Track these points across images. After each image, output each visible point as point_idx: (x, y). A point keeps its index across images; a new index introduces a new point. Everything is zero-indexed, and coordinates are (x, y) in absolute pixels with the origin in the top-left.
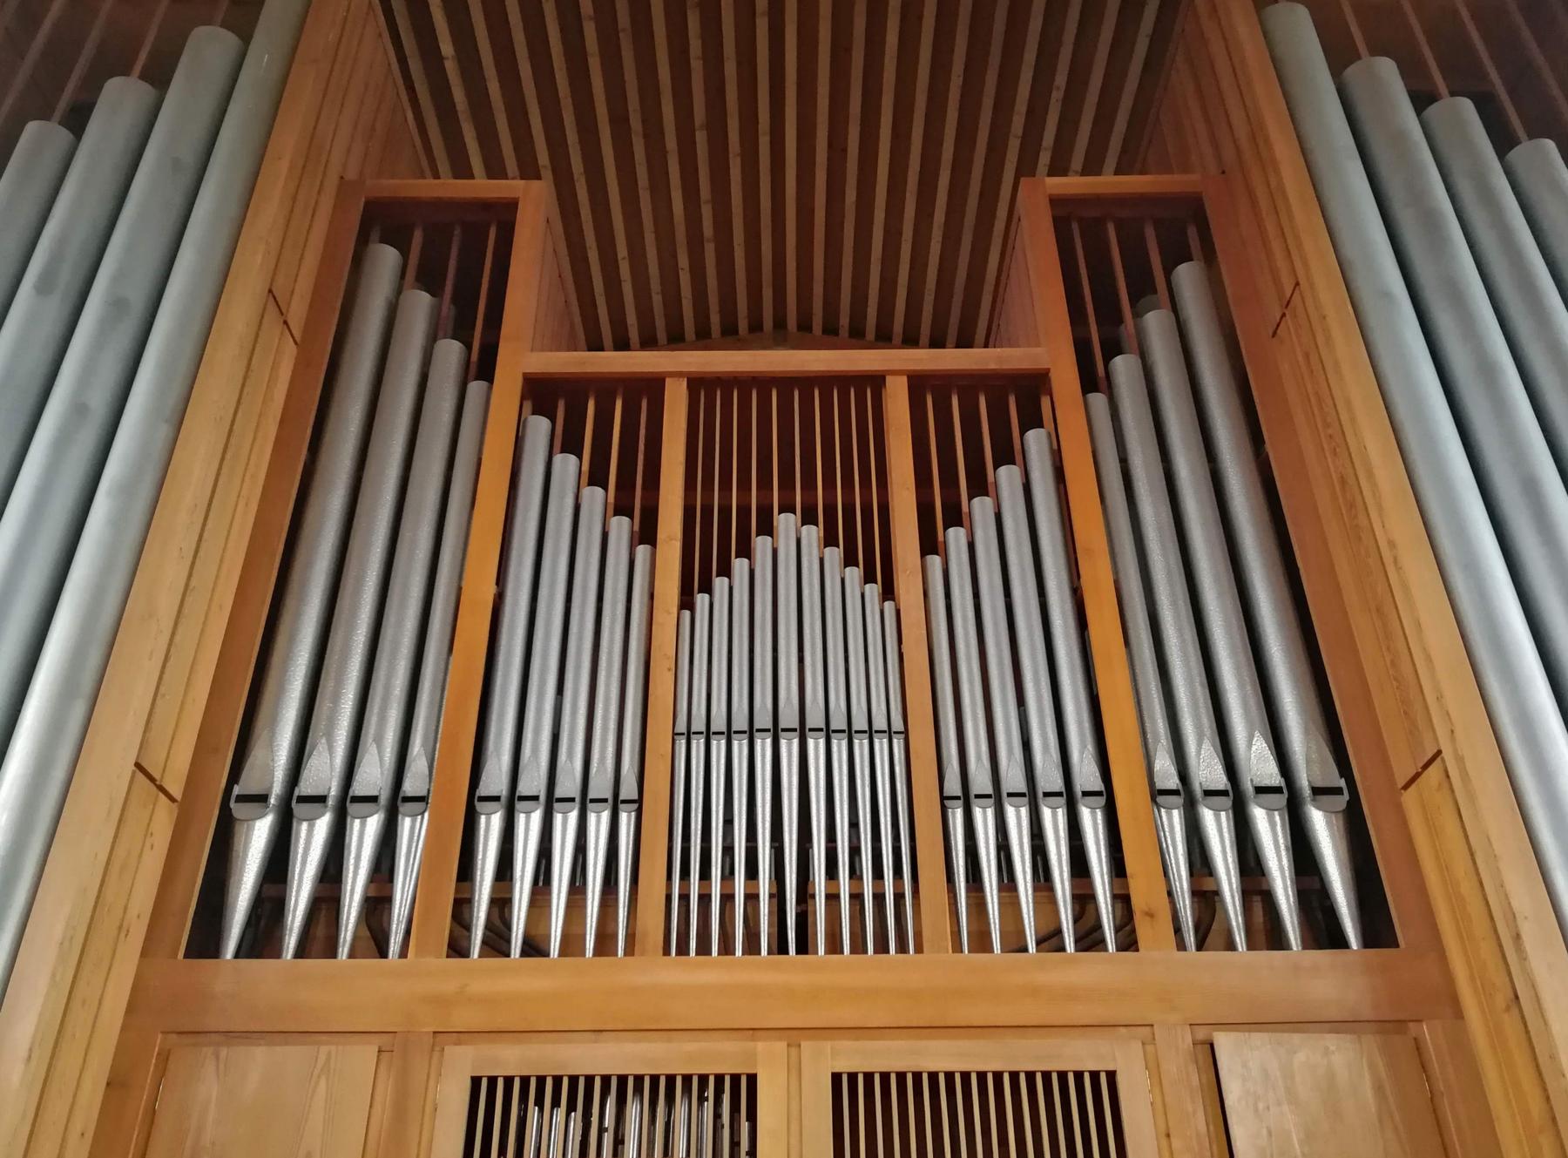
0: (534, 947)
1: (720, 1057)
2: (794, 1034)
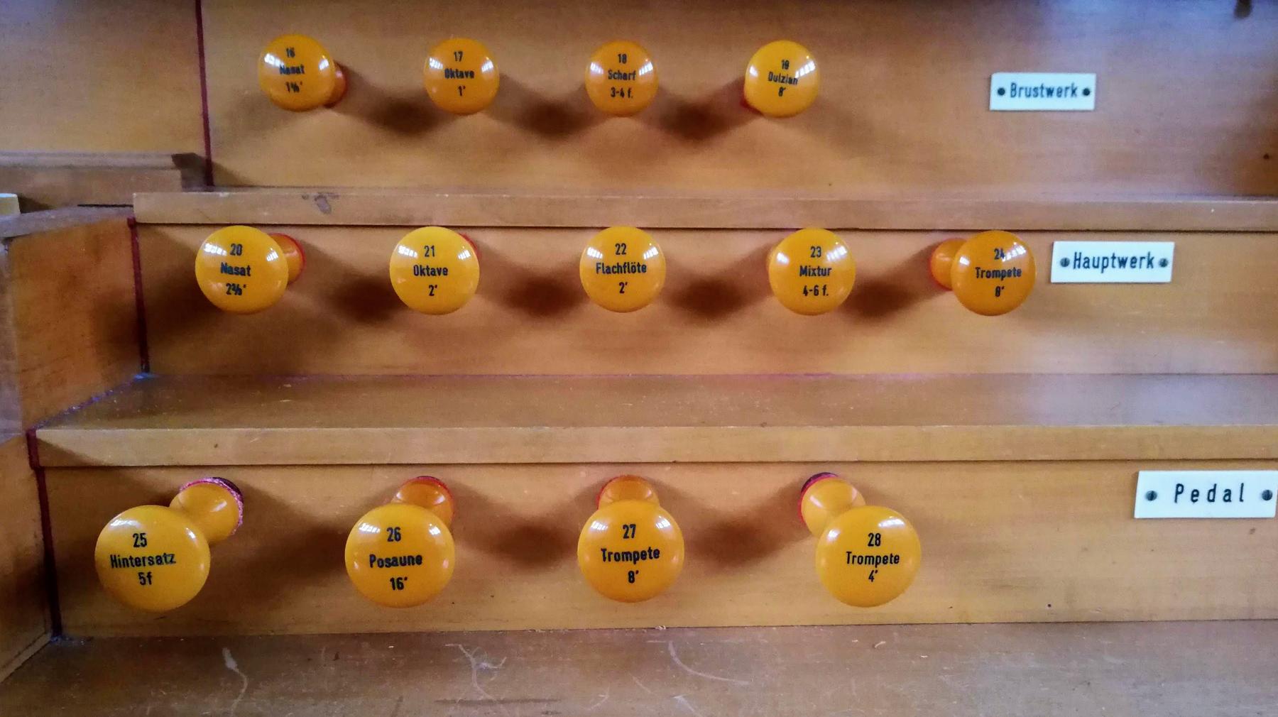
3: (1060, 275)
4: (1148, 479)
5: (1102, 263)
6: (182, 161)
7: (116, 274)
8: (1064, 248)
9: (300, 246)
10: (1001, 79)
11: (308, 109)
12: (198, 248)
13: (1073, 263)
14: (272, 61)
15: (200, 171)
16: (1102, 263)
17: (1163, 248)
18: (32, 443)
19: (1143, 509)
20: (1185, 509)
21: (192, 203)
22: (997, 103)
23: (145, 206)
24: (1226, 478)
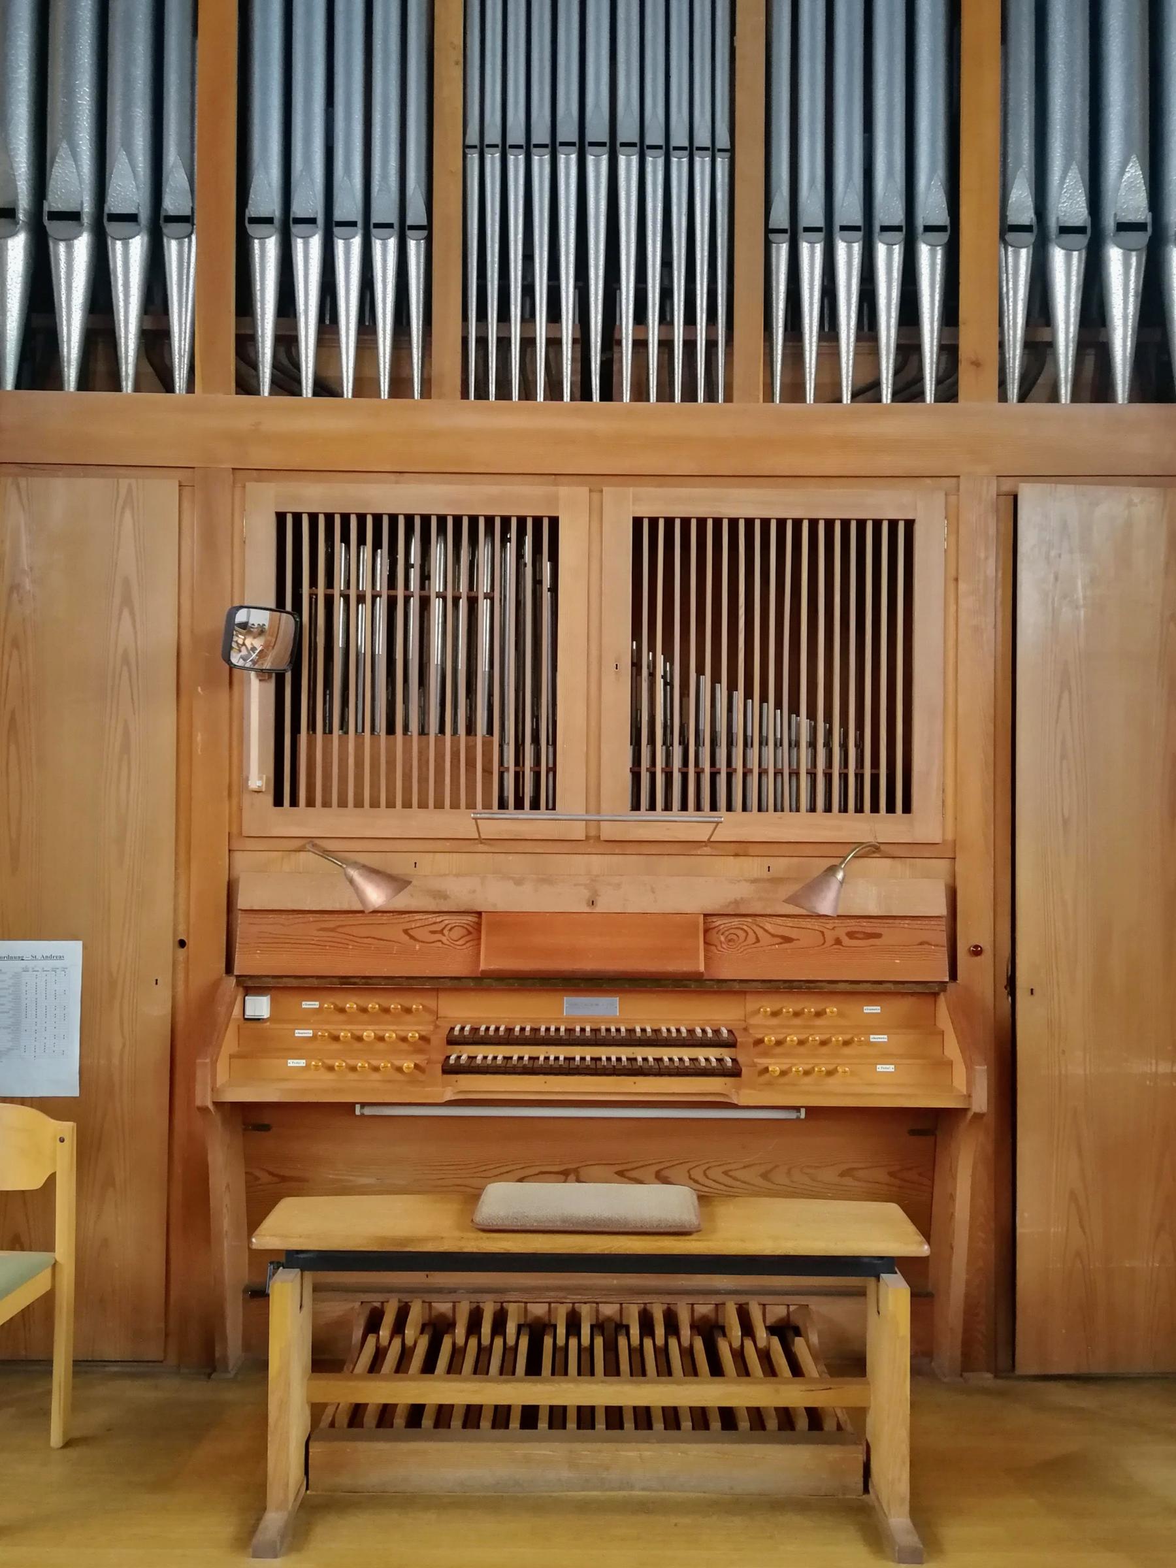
0: (326, 387)
1: (524, 500)
2: (595, 480)
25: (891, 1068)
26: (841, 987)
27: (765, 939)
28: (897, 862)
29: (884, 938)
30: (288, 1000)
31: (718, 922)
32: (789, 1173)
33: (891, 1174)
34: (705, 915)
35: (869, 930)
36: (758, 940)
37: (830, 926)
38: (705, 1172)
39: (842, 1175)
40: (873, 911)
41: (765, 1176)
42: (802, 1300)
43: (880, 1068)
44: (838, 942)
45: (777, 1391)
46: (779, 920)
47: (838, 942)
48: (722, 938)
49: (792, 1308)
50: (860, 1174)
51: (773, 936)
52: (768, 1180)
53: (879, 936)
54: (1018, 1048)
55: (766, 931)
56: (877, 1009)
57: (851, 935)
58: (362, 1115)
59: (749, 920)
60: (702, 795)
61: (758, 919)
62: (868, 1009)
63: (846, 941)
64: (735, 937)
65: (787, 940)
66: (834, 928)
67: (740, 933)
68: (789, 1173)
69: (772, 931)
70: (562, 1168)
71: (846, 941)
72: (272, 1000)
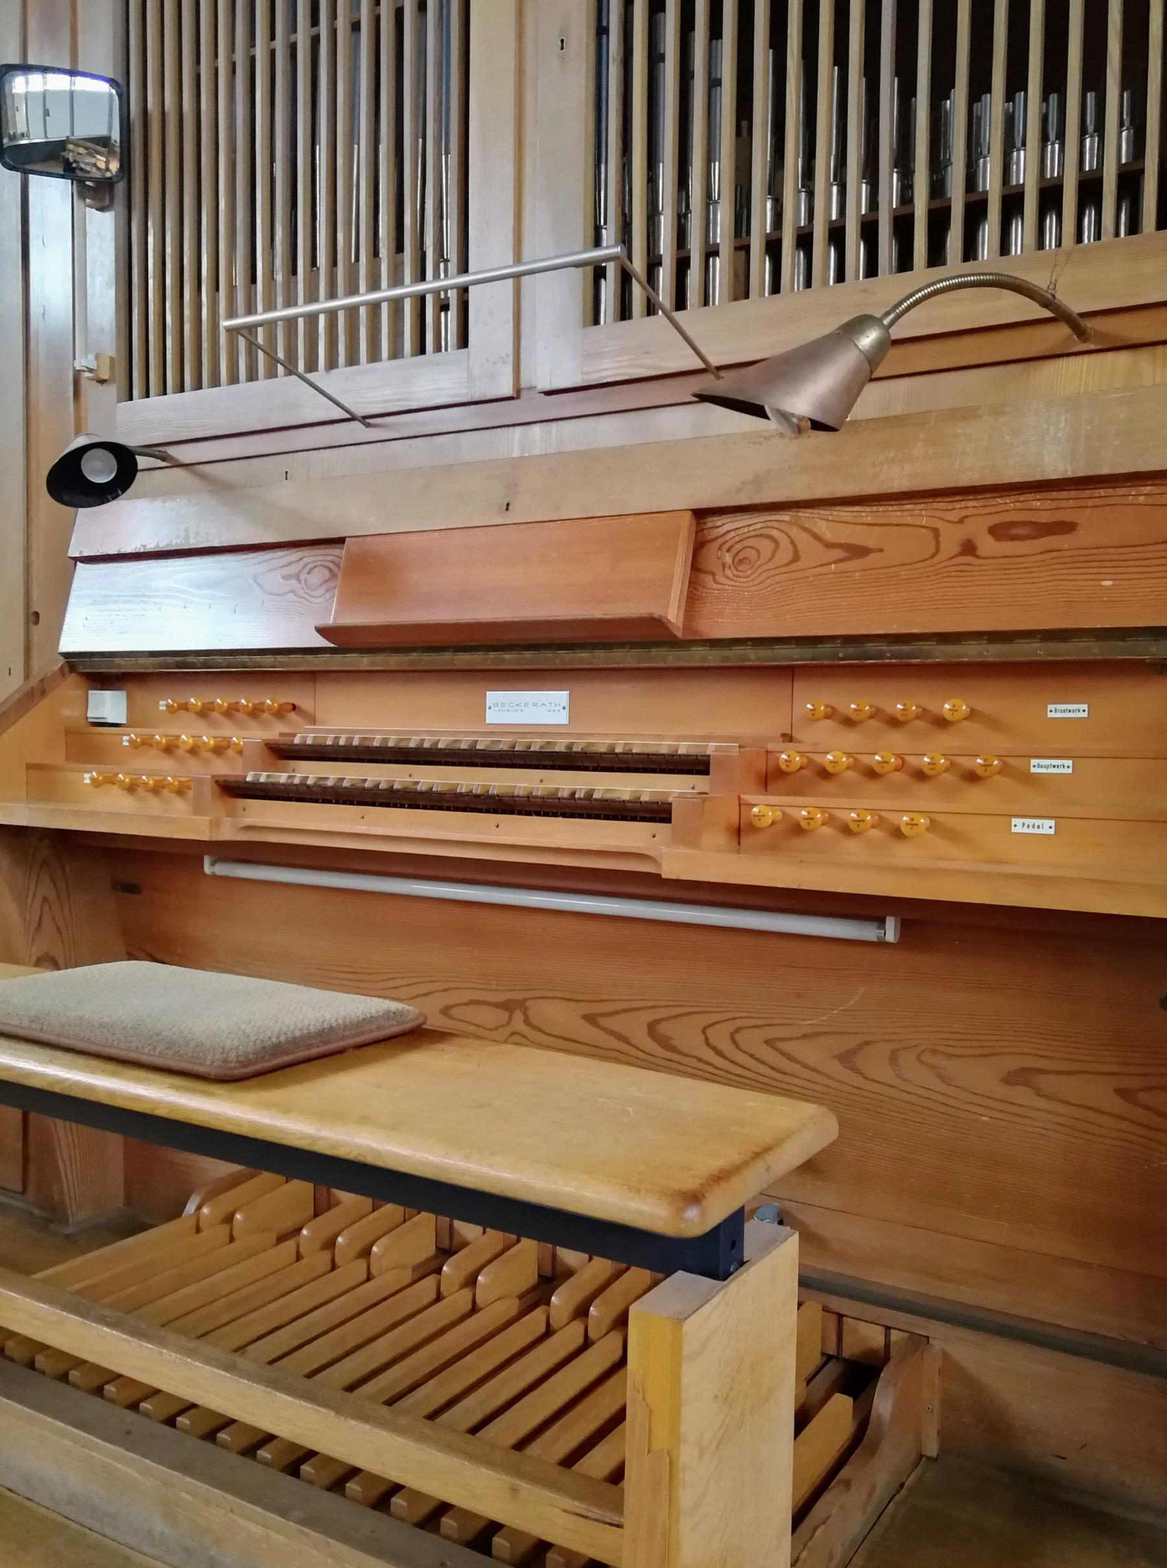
3: (1033, 770)
4: (1014, 821)
5: (1047, 767)
6: (784, 735)
7: (761, 765)
8: (1034, 762)
9: (880, 817)
10: (1050, 707)
11: (818, 720)
12: (902, 935)
13: (1038, 766)
14: (809, 706)
15: (788, 738)
16: (1047, 767)
17: (1069, 762)
18: (739, 798)
19: (1014, 830)
20: (1025, 830)
21: (781, 745)
22: (1050, 715)
23: (770, 747)
24: (1038, 822)
25: (1047, 827)
26: (971, 652)
27: (812, 552)
28: (1143, 356)
29: (1080, 532)
30: (144, 696)
31: (726, 524)
32: (894, 1057)
33: (1125, 1094)
34: (700, 514)
35: (1044, 518)
36: (796, 557)
37: (954, 516)
38: (732, 1036)
39: (1010, 1079)
40: (1055, 466)
41: (846, 1058)
42: (921, 1326)
43: (1019, 826)
44: (969, 548)
45: (514, 1491)
46: (845, 513)
47: (969, 548)
48: (728, 558)
49: (895, 1336)
50: (1050, 1083)
51: (829, 545)
52: (450, 1017)
53: (1067, 528)
54: (780, 635)
55: (816, 536)
56: (1078, 710)
57: (998, 532)
58: (214, 877)
59: (786, 516)
60: (140, 66)
61: (804, 514)
62: (1057, 711)
63: (987, 545)
64: (751, 554)
65: (857, 551)
66: (961, 521)
67: (766, 546)
68: (894, 1057)
69: (828, 536)
70: (502, 997)
71: (987, 545)
72: (128, 696)
